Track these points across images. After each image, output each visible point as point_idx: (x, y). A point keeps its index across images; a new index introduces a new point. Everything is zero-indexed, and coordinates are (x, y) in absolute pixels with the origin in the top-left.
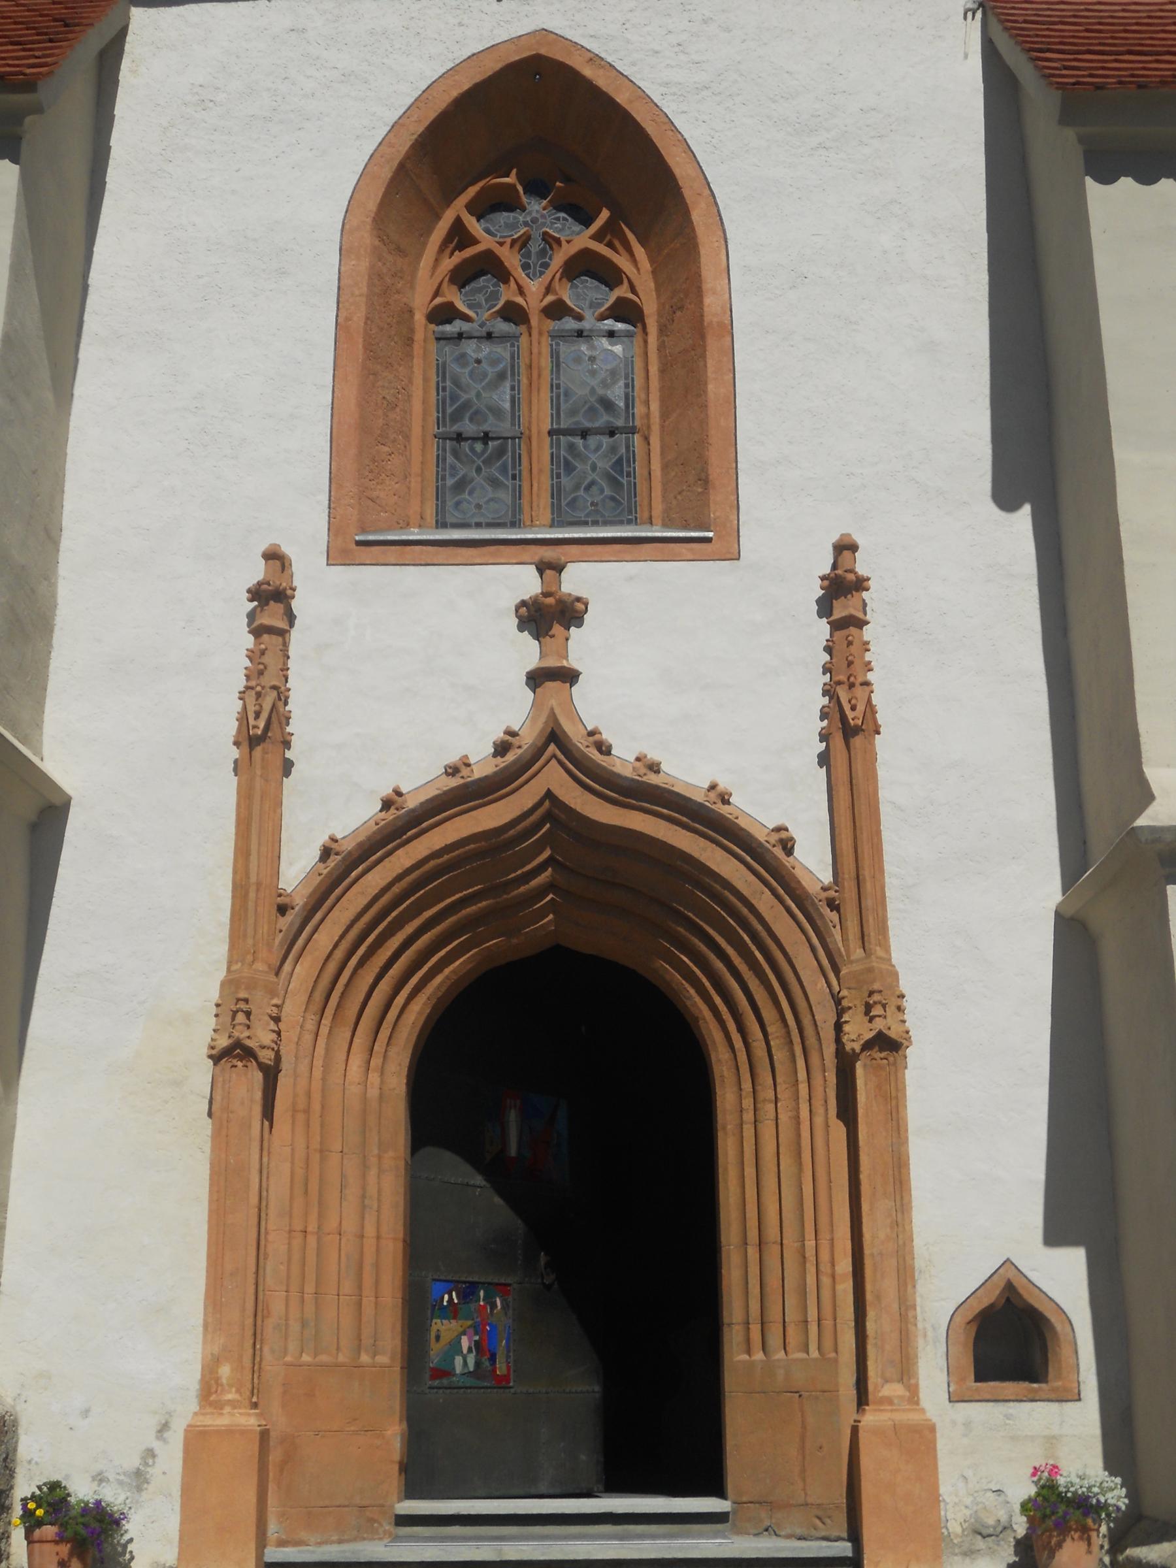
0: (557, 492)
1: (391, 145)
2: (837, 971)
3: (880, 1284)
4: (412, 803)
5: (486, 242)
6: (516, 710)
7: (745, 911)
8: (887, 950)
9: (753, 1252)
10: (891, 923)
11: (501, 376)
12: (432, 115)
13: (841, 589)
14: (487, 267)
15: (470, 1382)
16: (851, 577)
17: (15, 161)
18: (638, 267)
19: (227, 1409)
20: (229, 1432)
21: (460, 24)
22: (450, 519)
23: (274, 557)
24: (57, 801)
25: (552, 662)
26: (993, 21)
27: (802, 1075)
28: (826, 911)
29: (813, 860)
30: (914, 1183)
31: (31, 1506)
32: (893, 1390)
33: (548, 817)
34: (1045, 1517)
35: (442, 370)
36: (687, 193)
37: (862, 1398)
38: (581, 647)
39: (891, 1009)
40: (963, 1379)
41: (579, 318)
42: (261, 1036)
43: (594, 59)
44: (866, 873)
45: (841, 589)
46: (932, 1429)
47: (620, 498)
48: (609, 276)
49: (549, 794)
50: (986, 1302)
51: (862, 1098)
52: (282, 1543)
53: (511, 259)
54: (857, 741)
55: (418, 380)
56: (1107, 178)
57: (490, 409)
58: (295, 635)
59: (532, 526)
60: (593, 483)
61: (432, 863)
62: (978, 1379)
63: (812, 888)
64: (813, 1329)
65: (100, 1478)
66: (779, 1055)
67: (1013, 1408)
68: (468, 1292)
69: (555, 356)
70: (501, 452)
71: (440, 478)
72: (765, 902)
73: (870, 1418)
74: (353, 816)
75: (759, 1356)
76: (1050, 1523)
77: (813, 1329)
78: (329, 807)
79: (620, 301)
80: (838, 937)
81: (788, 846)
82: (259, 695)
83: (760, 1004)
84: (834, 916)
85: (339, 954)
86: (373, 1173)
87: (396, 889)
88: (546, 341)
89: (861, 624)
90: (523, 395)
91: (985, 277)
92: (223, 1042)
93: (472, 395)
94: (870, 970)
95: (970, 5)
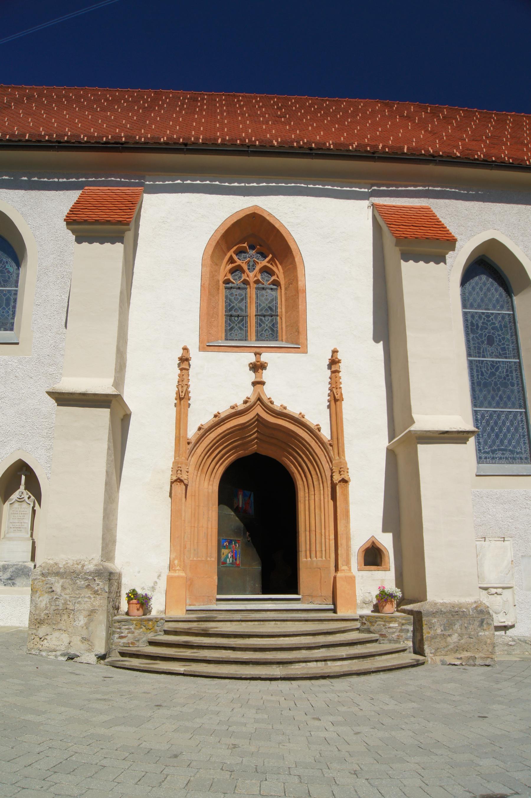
0: (257, 332)
1: (215, 236)
2: (331, 462)
3: (342, 541)
4: (222, 416)
5: (239, 262)
6: (248, 392)
7: (308, 446)
8: (345, 457)
9: (308, 533)
10: (345, 450)
11: (242, 299)
12: (226, 228)
13: (334, 362)
14: (237, 270)
15: (231, 565)
16: (337, 360)
17: (122, 243)
18: (279, 271)
19: (177, 571)
20: (178, 577)
21: (234, 203)
22: (228, 338)
23: (185, 349)
24: (128, 413)
25: (258, 380)
26: (375, 209)
27: (322, 488)
28: (329, 446)
29: (326, 433)
30: (351, 516)
31: (130, 595)
32: (345, 568)
33: (257, 420)
34: (382, 599)
35: (226, 297)
36: (294, 253)
37: (337, 569)
38: (266, 375)
39: (345, 472)
40: (361, 565)
41: (263, 284)
42: (184, 477)
43: (270, 214)
44: (340, 437)
45: (334, 362)
46: (354, 577)
47: (273, 335)
48: (271, 273)
49: (257, 414)
50: (367, 546)
51: (338, 494)
52: (190, 605)
53: (245, 267)
54: (338, 403)
55: (221, 300)
56: (406, 260)
57: (239, 308)
58: (190, 370)
59: (251, 341)
60: (267, 329)
61: (227, 432)
62: (365, 565)
63: (326, 441)
64: (324, 552)
65: (143, 589)
66: (315, 483)
67: (374, 572)
68: (230, 542)
69: (257, 294)
70: (242, 320)
71: (226, 327)
72: (313, 444)
73: (339, 575)
74: (207, 419)
75: (309, 559)
76: (383, 600)
77: (324, 552)
78: (200, 416)
79: (274, 280)
80: (332, 454)
81: (319, 430)
82: (182, 387)
83: (311, 470)
84: (331, 448)
85: (203, 455)
86: (210, 511)
87: (218, 438)
88: (254, 290)
89: (339, 372)
90: (248, 305)
91: (372, 280)
92: (175, 478)
93: (235, 305)
94: (341, 462)
95: (370, 205)
